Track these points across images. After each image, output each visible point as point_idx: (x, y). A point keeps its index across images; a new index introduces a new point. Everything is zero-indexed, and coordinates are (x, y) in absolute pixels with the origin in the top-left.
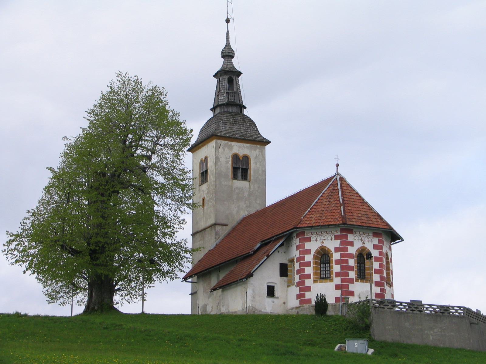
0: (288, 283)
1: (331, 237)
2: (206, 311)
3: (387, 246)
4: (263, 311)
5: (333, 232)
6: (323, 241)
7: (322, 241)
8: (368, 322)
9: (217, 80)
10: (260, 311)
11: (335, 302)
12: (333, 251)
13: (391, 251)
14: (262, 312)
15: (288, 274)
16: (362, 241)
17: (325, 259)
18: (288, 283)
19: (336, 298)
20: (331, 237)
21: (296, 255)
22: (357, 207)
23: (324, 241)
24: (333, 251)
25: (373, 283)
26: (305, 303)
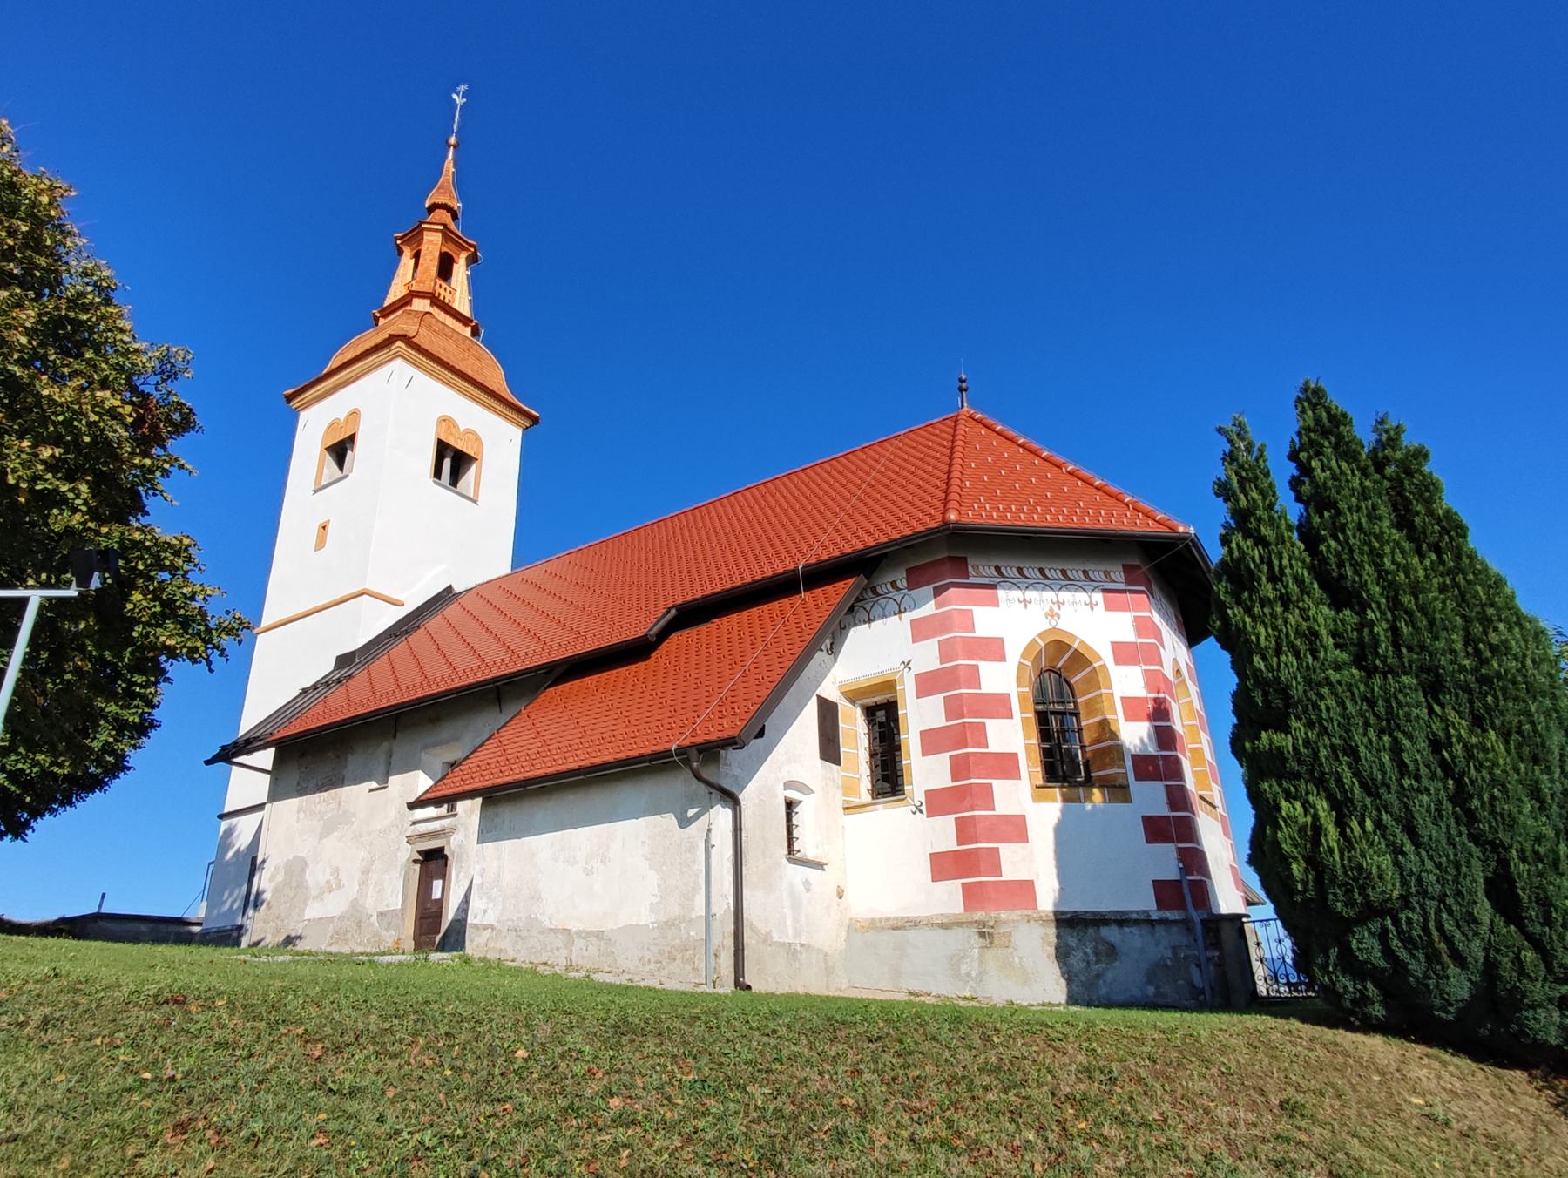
0: (844, 795)
1: (899, 606)
5: (1092, 577)
6: (1055, 607)
7: (1051, 610)
11: (962, 910)
12: (1107, 656)
15: (842, 750)
18: (844, 795)
19: (1158, 885)
20: (899, 606)
22: (910, 499)
23: (1059, 608)
24: (1107, 656)
25: (238, 851)
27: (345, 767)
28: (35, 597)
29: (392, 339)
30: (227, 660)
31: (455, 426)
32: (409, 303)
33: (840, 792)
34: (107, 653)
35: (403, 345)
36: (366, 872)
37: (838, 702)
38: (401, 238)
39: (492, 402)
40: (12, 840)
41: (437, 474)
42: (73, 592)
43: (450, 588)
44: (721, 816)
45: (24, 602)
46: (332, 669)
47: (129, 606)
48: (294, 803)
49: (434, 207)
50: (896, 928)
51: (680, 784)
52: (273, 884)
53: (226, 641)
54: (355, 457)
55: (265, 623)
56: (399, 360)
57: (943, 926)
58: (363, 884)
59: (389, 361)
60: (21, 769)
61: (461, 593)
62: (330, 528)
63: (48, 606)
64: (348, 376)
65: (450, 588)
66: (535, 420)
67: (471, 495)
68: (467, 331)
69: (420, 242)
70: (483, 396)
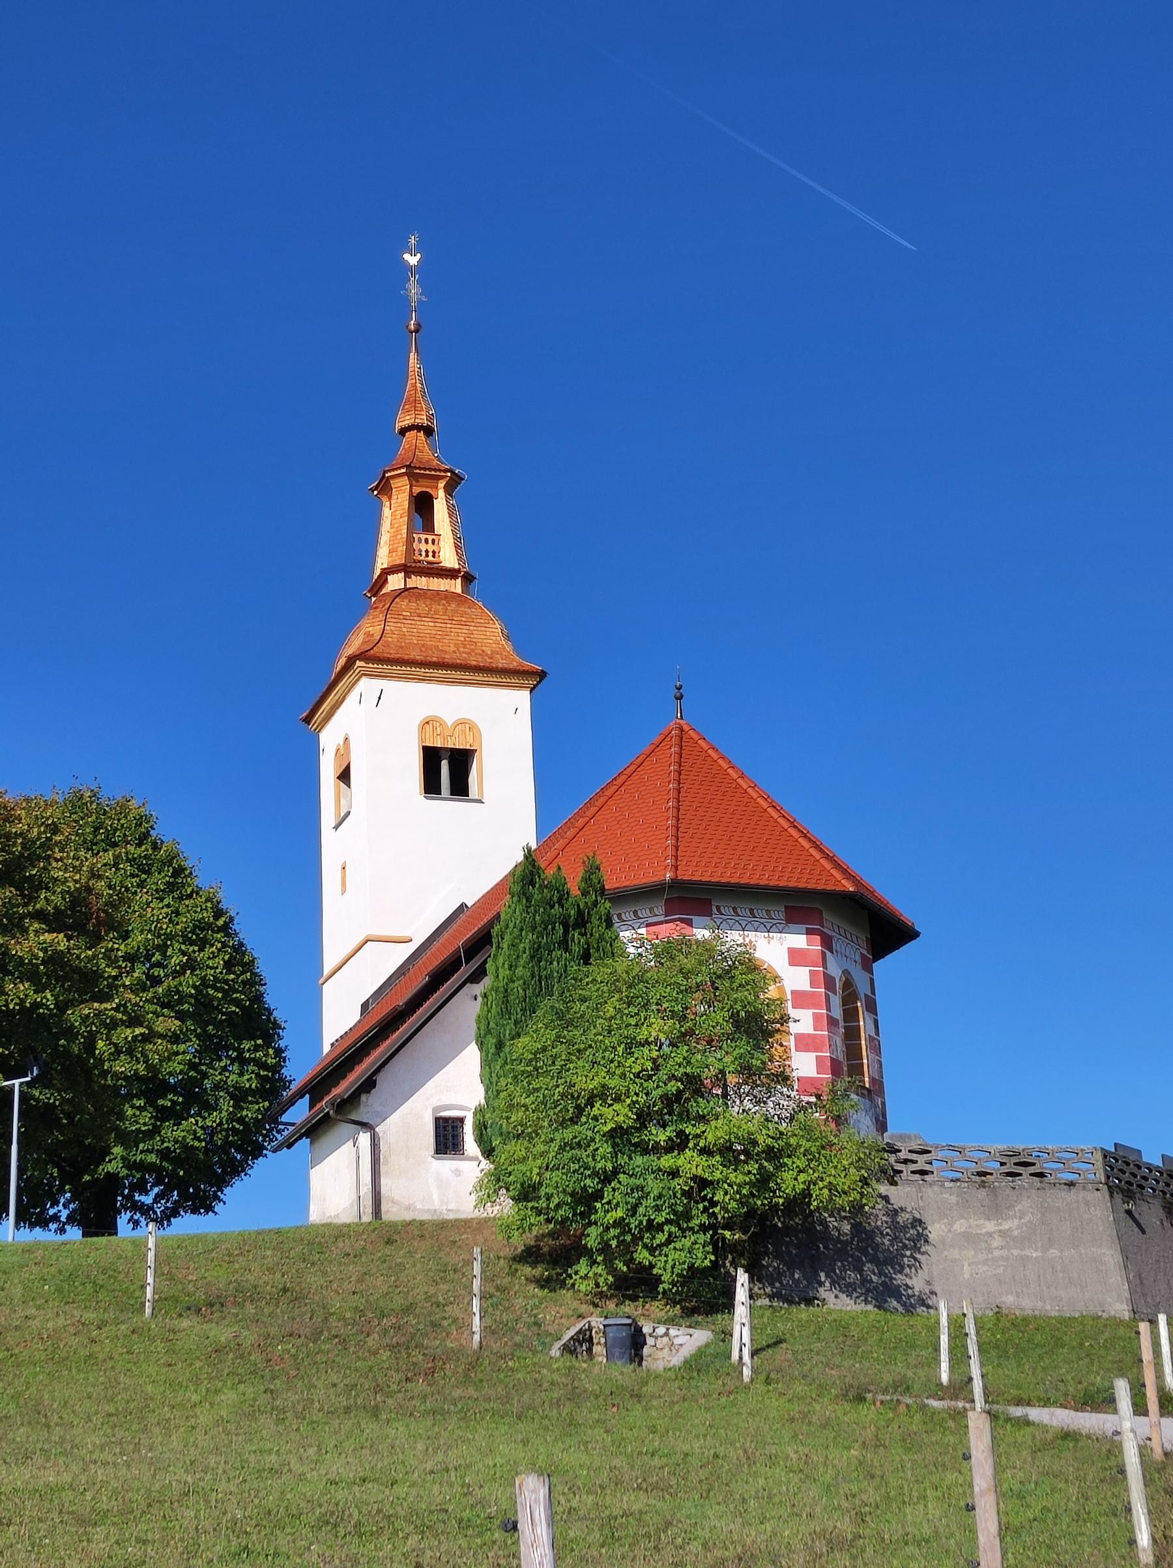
4: (419, 1206)
10: (408, 1208)
28: (17, 1082)
29: (351, 661)
31: (442, 723)
32: (386, 581)
34: (211, 1027)
35: (362, 664)
38: (376, 488)
39: (480, 677)
41: (431, 786)
44: (364, 1138)
47: (97, 1052)
49: (403, 431)
56: (364, 679)
60: (167, 1147)
62: (347, 868)
63: (21, 1084)
64: (337, 698)
66: (542, 675)
67: (477, 797)
68: (456, 586)
70: (467, 676)
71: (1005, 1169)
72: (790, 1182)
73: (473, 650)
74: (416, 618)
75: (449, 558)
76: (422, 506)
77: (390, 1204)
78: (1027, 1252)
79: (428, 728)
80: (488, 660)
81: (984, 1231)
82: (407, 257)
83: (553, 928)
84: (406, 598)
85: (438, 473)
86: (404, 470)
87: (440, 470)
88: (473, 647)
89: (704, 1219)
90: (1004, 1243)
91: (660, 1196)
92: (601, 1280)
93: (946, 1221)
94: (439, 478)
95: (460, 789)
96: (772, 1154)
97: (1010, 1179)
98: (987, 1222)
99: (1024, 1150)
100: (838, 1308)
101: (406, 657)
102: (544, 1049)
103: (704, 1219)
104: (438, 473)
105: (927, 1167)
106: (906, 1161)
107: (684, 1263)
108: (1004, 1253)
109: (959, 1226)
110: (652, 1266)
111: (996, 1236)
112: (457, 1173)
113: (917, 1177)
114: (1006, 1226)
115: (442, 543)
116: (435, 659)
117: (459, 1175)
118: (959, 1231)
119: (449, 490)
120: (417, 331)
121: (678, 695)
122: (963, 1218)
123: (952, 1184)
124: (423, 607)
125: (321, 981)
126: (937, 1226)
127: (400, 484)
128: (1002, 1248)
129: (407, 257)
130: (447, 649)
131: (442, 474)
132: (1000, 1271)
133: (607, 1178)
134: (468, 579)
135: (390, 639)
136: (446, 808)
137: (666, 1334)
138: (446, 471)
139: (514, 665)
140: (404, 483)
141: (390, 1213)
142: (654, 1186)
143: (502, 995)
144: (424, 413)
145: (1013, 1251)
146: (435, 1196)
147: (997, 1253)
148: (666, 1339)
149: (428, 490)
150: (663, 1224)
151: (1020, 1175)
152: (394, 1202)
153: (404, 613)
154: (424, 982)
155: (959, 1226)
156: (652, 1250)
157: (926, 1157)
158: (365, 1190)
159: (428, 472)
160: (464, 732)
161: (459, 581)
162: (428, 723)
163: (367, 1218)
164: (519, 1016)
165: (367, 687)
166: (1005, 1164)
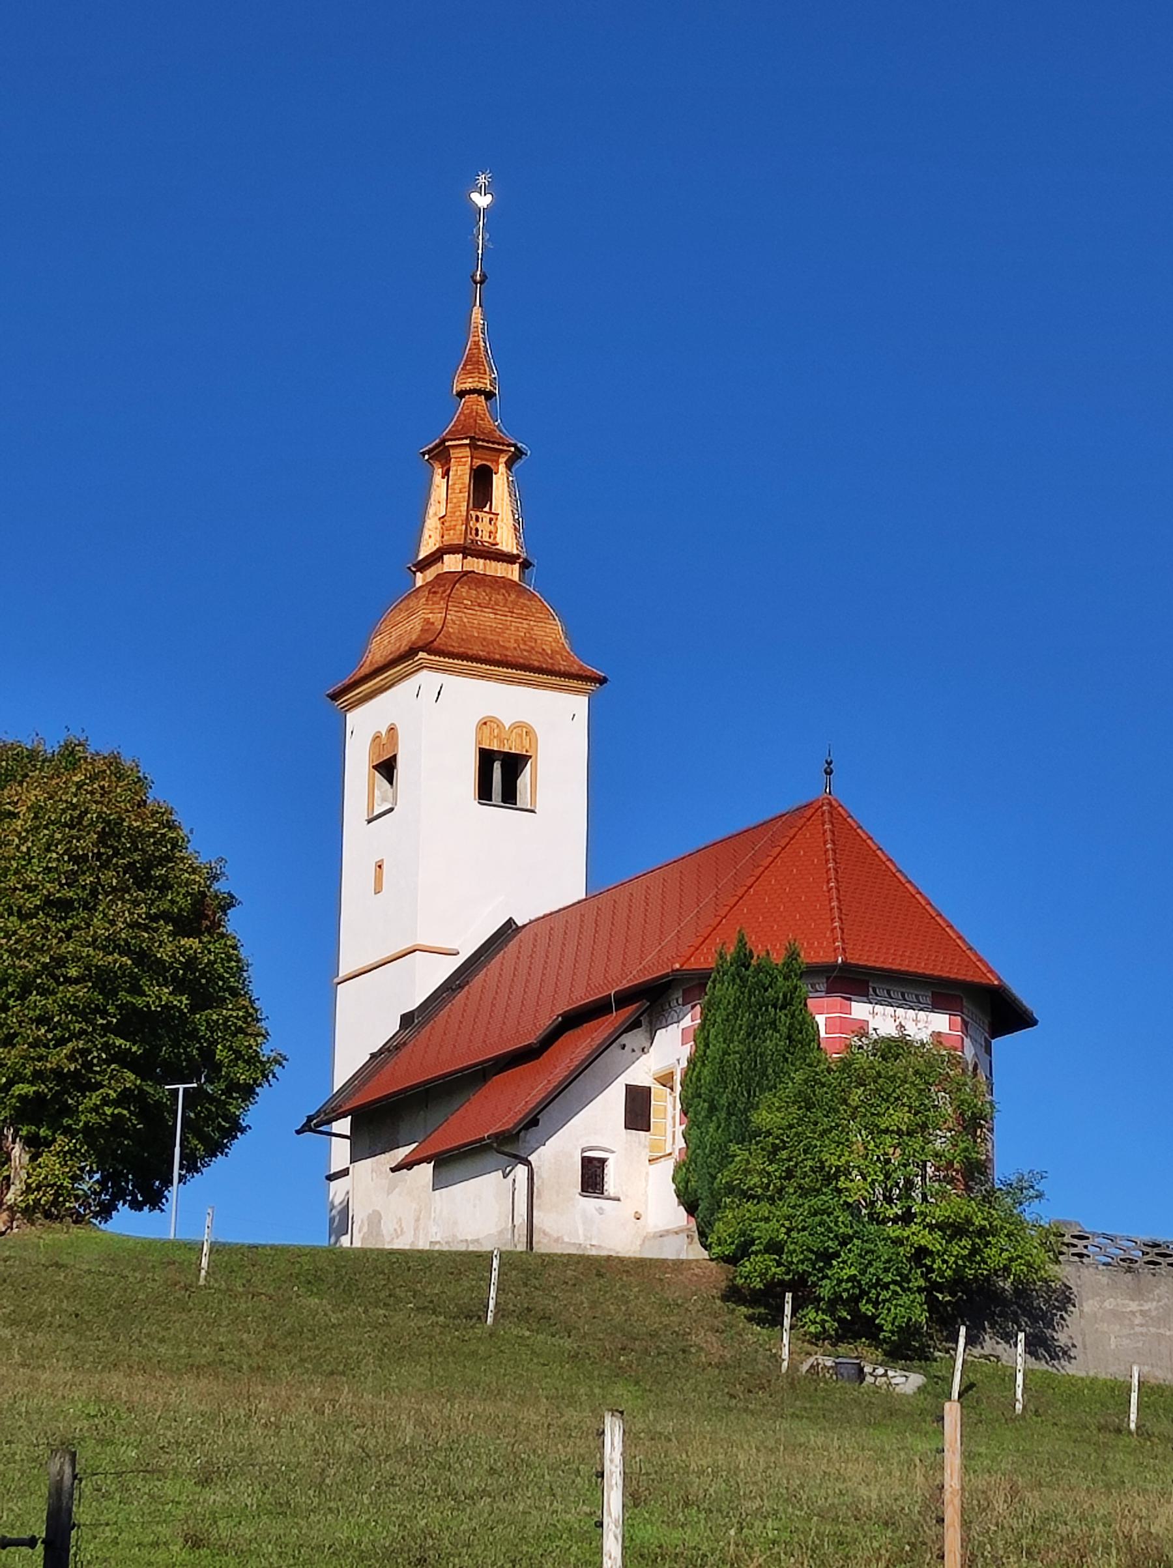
2: (379, 1234)
3: (979, 1040)
4: (566, 1239)
8: (940, 1514)
9: (584, 897)
10: (557, 1240)
13: (991, 1056)
14: (563, 1242)
16: (897, 1023)
17: (738, 901)
21: (678, 1060)
26: (498, 660)
27: (398, 1133)
28: (181, 1087)
30: (250, 1128)
31: (500, 725)
32: (440, 559)
33: (647, 1150)
36: (418, 1220)
37: (652, 1086)
40: (151, 1211)
41: (484, 794)
42: (195, 1085)
43: (510, 921)
45: (178, 1089)
46: (398, 1028)
48: (369, 1162)
49: (462, 394)
50: (661, 1236)
51: (495, 1158)
52: (362, 1234)
53: (276, 1068)
54: (402, 771)
55: (343, 972)
57: (676, 1233)
58: (416, 1229)
59: (412, 673)
61: (525, 926)
62: (385, 867)
64: (383, 683)
65: (510, 921)
66: (602, 681)
67: (529, 807)
68: (513, 572)
69: (448, 460)
71: (1147, 1258)
72: (994, 1257)
73: (533, 648)
74: (477, 608)
75: (507, 542)
76: (482, 480)
77: (542, 1235)
78: (1161, 1331)
79: (486, 729)
80: (550, 661)
81: (1128, 1310)
82: (475, 196)
83: (767, 1010)
84: (466, 583)
85: (501, 447)
86: (467, 441)
87: (503, 444)
88: (533, 644)
89: (922, 1283)
90: (1144, 1322)
91: (889, 1261)
92: (827, 1325)
93: (1098, 1298)
94: (502, 451)
95: (510, 797)
96: (982, 1232)
97: (1152, 1267)
98: (1131, 1303)
99: (1164, 1243)
100: (1010, 1364)
101: (470, 653)
102: (791, 1127)
103: (922, 1283)
104: (501, 447)
105: (1085, 1251)
106: (1068, 1245)
107: (904, 1317)
108: (1144, 1330)
109: (1109, 1304)
110: (874, 1317)
111: (1138, 1314)
112: (601, 1211)
113: (1076, 1259)
114: (1146, 1307)
115: (499, 523)
116: (497, 657)
117: (601, 1214)
118: (1109, 1307)
119: (509, 465)
120: (481, 282)
121: (828, 770)
122: (1112, 1297)
123: (1104, 1267)
124: (483, 597)
125: (336, 980)
126: (1091, 1302)
127: (460, 455)
128: (1142, 1325)
129: (475, 196)
130: (507, 645)
131: (505, 448)
132: (1140, 1345)
133: (844, 1241)
134: (525, 565)
135: (451, 630)
136: (497, 815)
137: (885, 1375)
138: (509, 445)
139: (574, 669)
140: (465, 454)
141: (542, 1246)
142: (884, 1251)
143: (718, 1066)
144: (487, 376)
145: (1151, 1329)
146: (581, 1232)
147: (1138, 1329)
148: (884, 1379)
149: (489, 464)
150: (889, 1283)
151: (1160, 1264)
152: (545, 1234)
153: (465, 602)
154: (557, 1022)
155: (1109, 1304)
156: (876, 1304)
157: (1085, 1242)
158: (521, 1220)
159: (490, 445)
160: (521, 736)
161: (517, 566)
162: (485, 723)
163: (522, 1247)
164: (736, 1087)
165: (428, 680)
166: (1148, 1253)
